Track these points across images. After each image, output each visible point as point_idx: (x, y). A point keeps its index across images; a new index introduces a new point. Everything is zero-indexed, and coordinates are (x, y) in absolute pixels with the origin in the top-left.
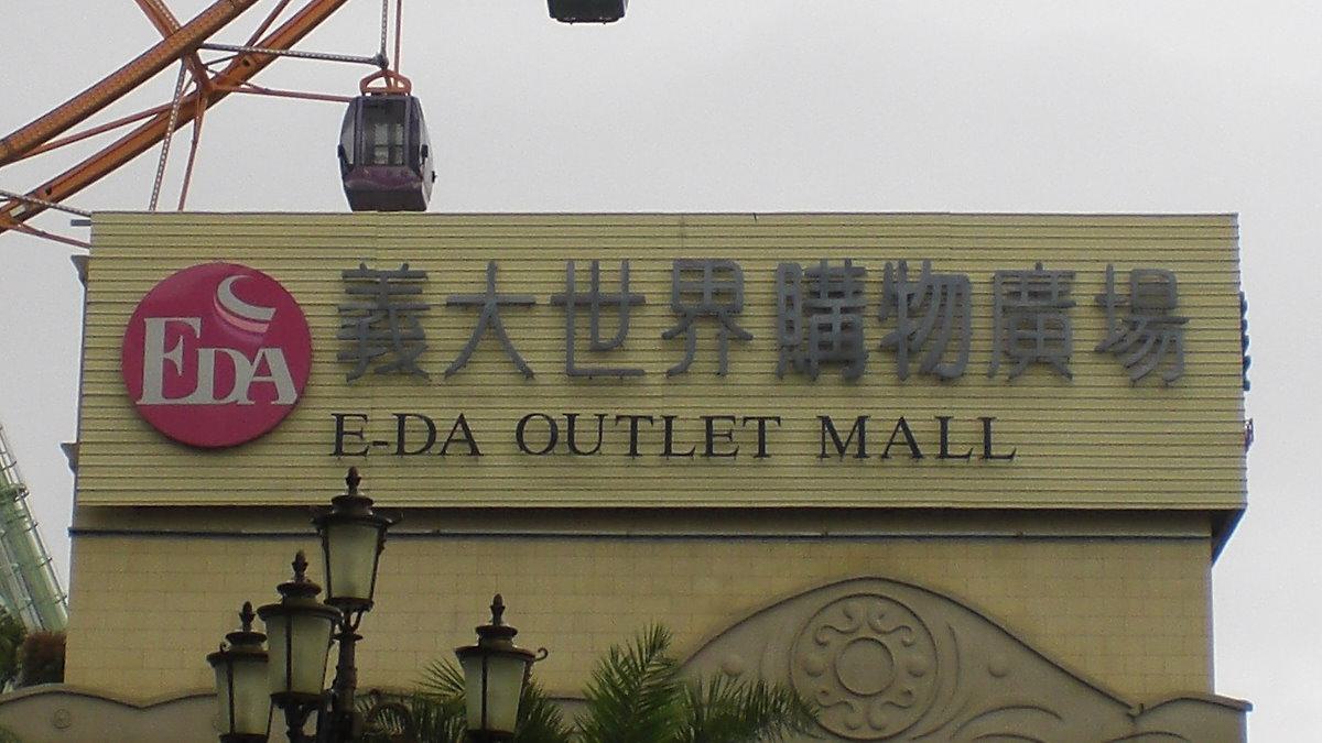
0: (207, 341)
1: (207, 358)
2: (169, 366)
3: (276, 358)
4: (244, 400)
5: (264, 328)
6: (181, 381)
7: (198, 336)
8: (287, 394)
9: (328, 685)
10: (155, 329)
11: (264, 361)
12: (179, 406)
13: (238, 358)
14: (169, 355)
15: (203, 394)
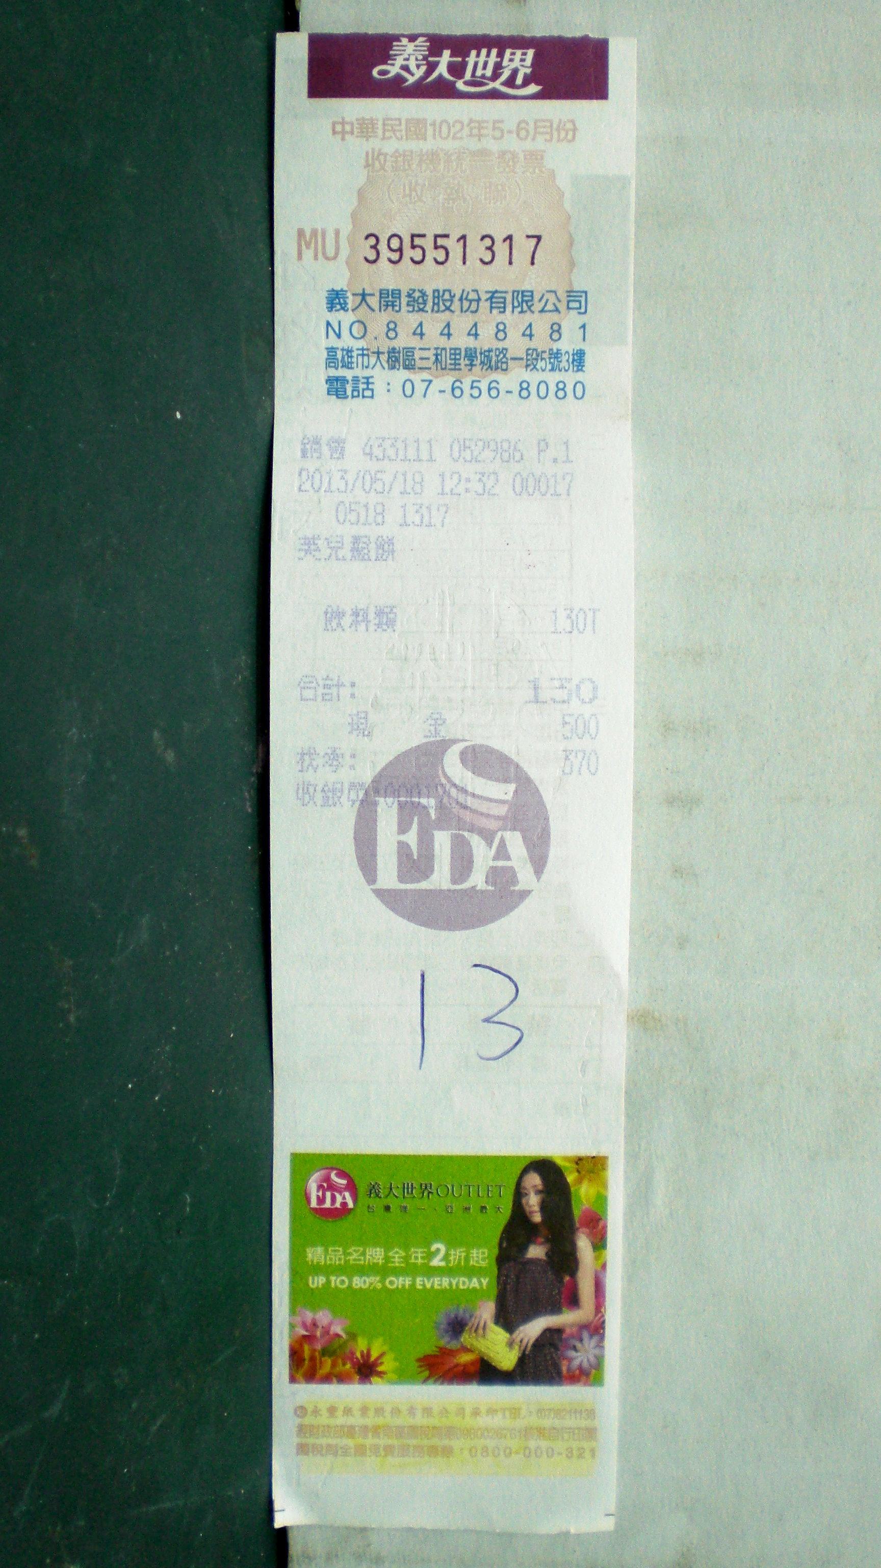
0: (444, 821)
1: (328, 1194)
2: (403, 848)
3: (347, 1194)
4: (481, 885)
5: (502, 810)
6: (415, 864)
7: (433, 816)
8: (351, 1205)
9: (310, 1278)
10: (387, 813)
11: (502, 841)
12: (419, 892)
13: (476, 841)
14: (403, 838)
15: (328, 1204)
